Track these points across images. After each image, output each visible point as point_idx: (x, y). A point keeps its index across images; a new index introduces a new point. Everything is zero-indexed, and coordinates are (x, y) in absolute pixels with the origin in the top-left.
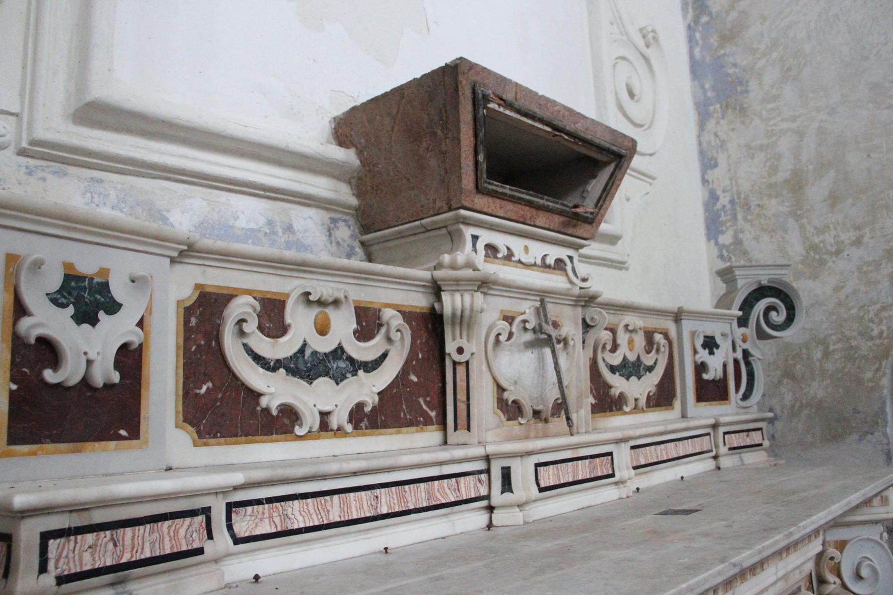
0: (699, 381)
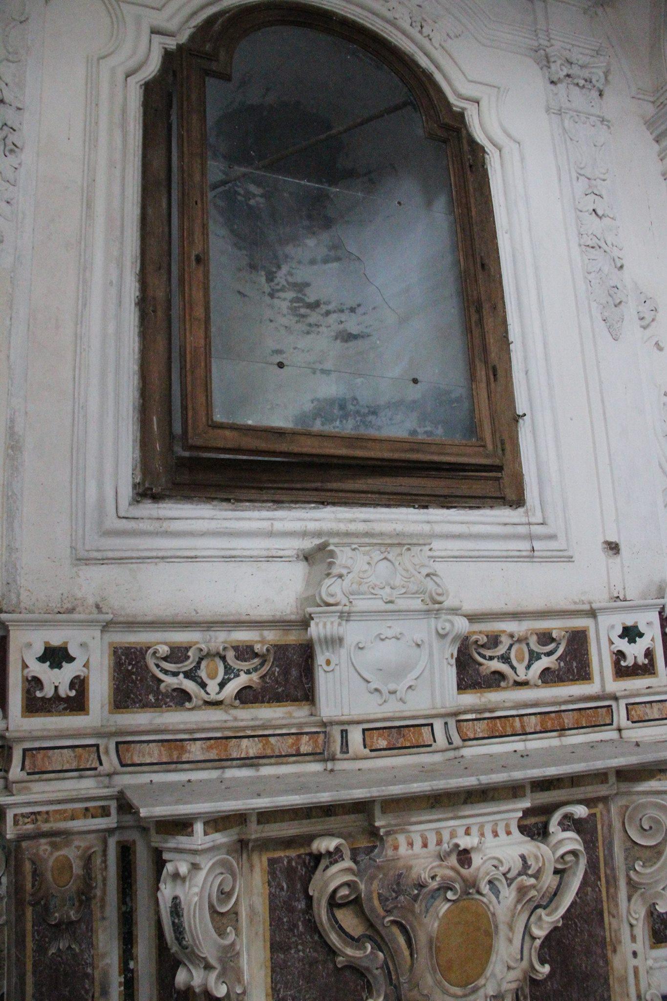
0: (616, 664)
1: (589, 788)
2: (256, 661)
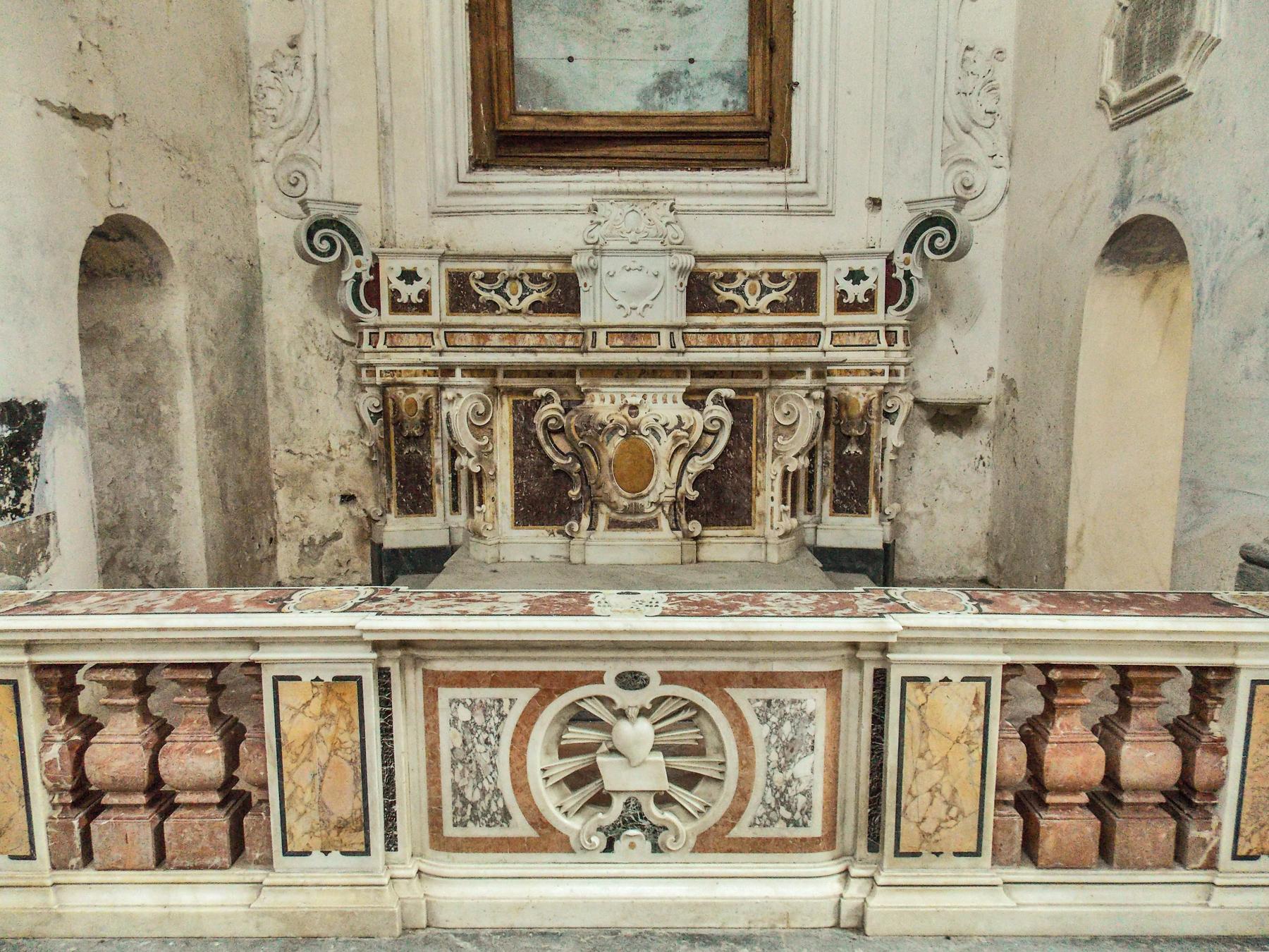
1: (747, 380)
2: (545, 284)
